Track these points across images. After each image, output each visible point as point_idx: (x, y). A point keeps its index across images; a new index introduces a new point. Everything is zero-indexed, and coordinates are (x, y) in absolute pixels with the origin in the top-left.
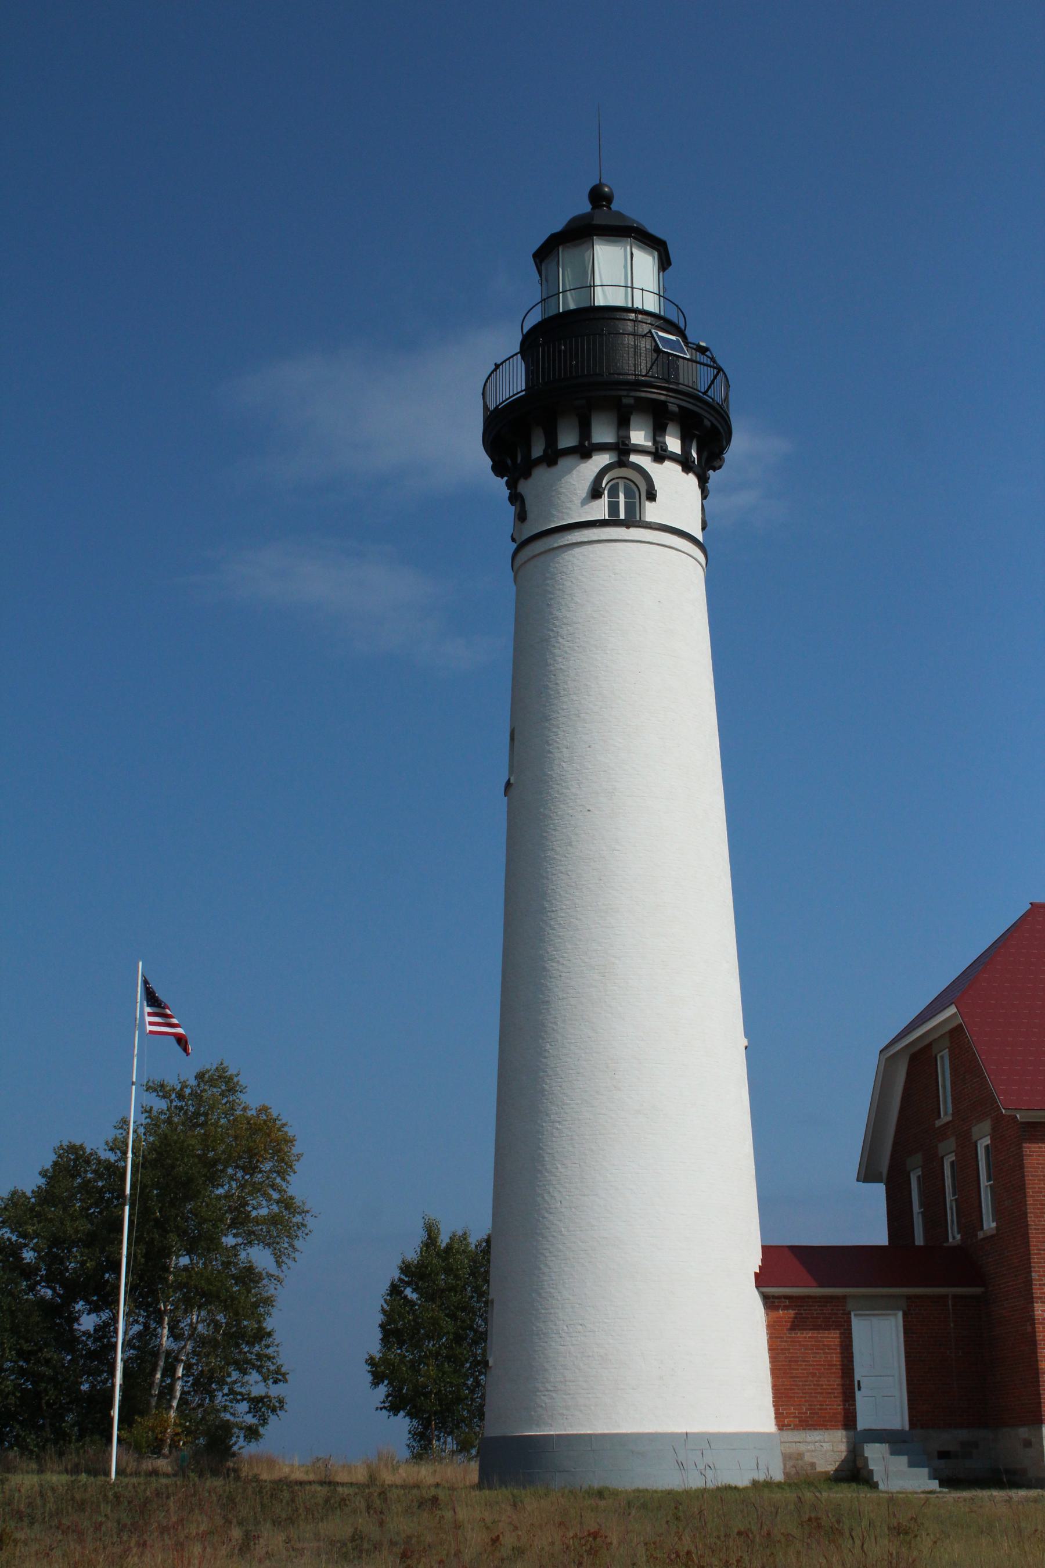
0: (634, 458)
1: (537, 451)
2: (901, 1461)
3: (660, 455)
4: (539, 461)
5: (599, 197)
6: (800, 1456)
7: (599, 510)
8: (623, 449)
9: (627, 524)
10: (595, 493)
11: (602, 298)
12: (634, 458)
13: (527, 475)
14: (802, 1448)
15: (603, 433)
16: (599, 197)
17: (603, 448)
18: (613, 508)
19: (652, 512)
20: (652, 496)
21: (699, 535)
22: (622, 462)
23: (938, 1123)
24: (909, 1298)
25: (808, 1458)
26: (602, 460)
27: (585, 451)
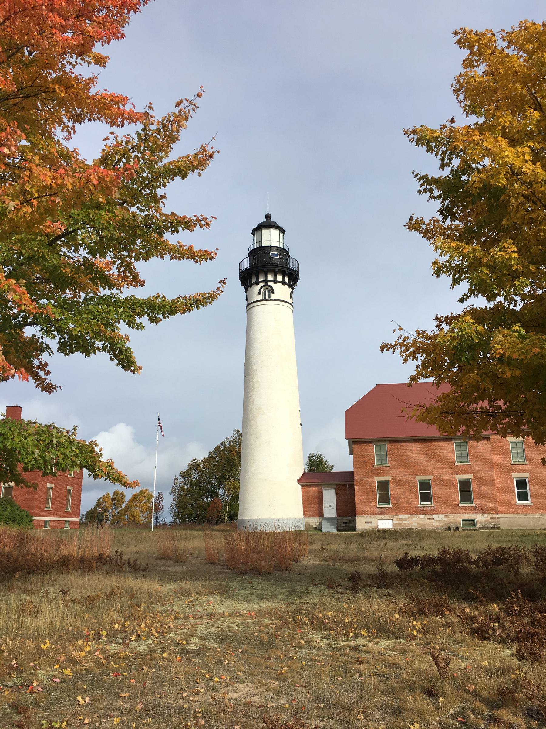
0: (269, 283)
1: (254, 281)
2: (329, 525)
3: (275, 281)
4: (254, 283)
5: (268, 217)
6: (309, 523)
7: (261, 297)
8: (266, 281)
9: (267, 300)
10: (260, 293)
11: (264, 244)
12: (269, 283)
13: (251, 286)
14: (309, 521)
15: (262, 279)
16: (268, 217)
17: (261, 282)
18: (265, 296)
19: (273, 296)
20: (273, 292)
21: (290, 301)
22: (266, 285)
23: (518, 373)
24: (337, 485)
25: (311, 524)
26: (261, 285)
27: (257, 283)
